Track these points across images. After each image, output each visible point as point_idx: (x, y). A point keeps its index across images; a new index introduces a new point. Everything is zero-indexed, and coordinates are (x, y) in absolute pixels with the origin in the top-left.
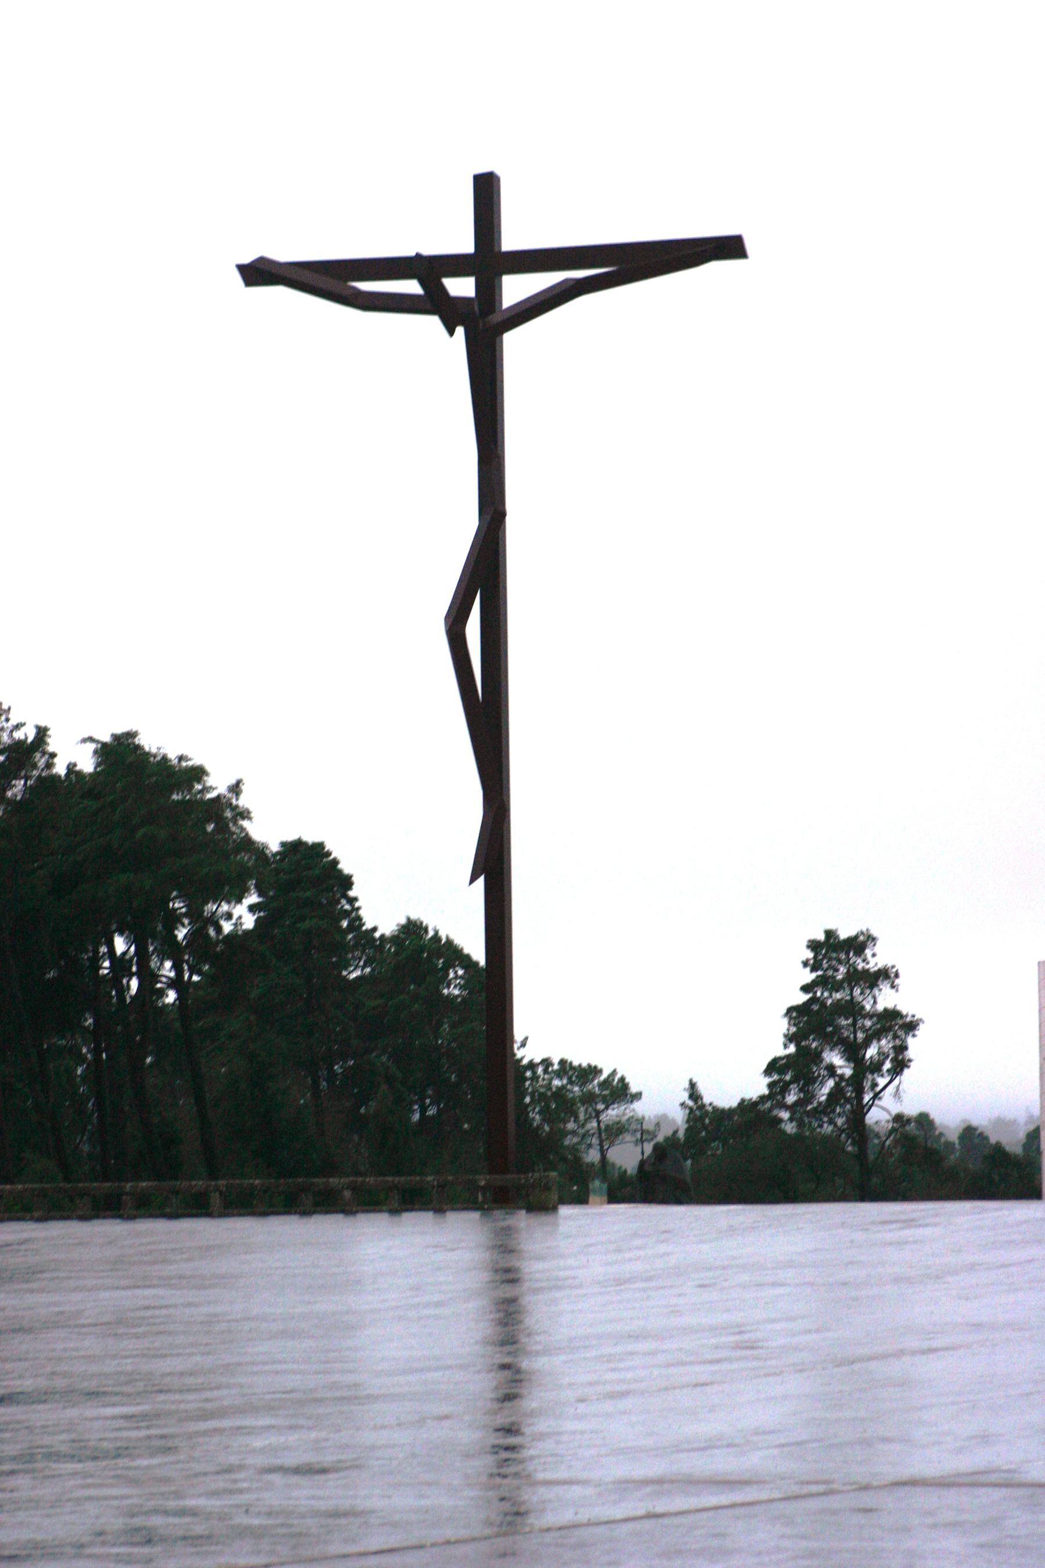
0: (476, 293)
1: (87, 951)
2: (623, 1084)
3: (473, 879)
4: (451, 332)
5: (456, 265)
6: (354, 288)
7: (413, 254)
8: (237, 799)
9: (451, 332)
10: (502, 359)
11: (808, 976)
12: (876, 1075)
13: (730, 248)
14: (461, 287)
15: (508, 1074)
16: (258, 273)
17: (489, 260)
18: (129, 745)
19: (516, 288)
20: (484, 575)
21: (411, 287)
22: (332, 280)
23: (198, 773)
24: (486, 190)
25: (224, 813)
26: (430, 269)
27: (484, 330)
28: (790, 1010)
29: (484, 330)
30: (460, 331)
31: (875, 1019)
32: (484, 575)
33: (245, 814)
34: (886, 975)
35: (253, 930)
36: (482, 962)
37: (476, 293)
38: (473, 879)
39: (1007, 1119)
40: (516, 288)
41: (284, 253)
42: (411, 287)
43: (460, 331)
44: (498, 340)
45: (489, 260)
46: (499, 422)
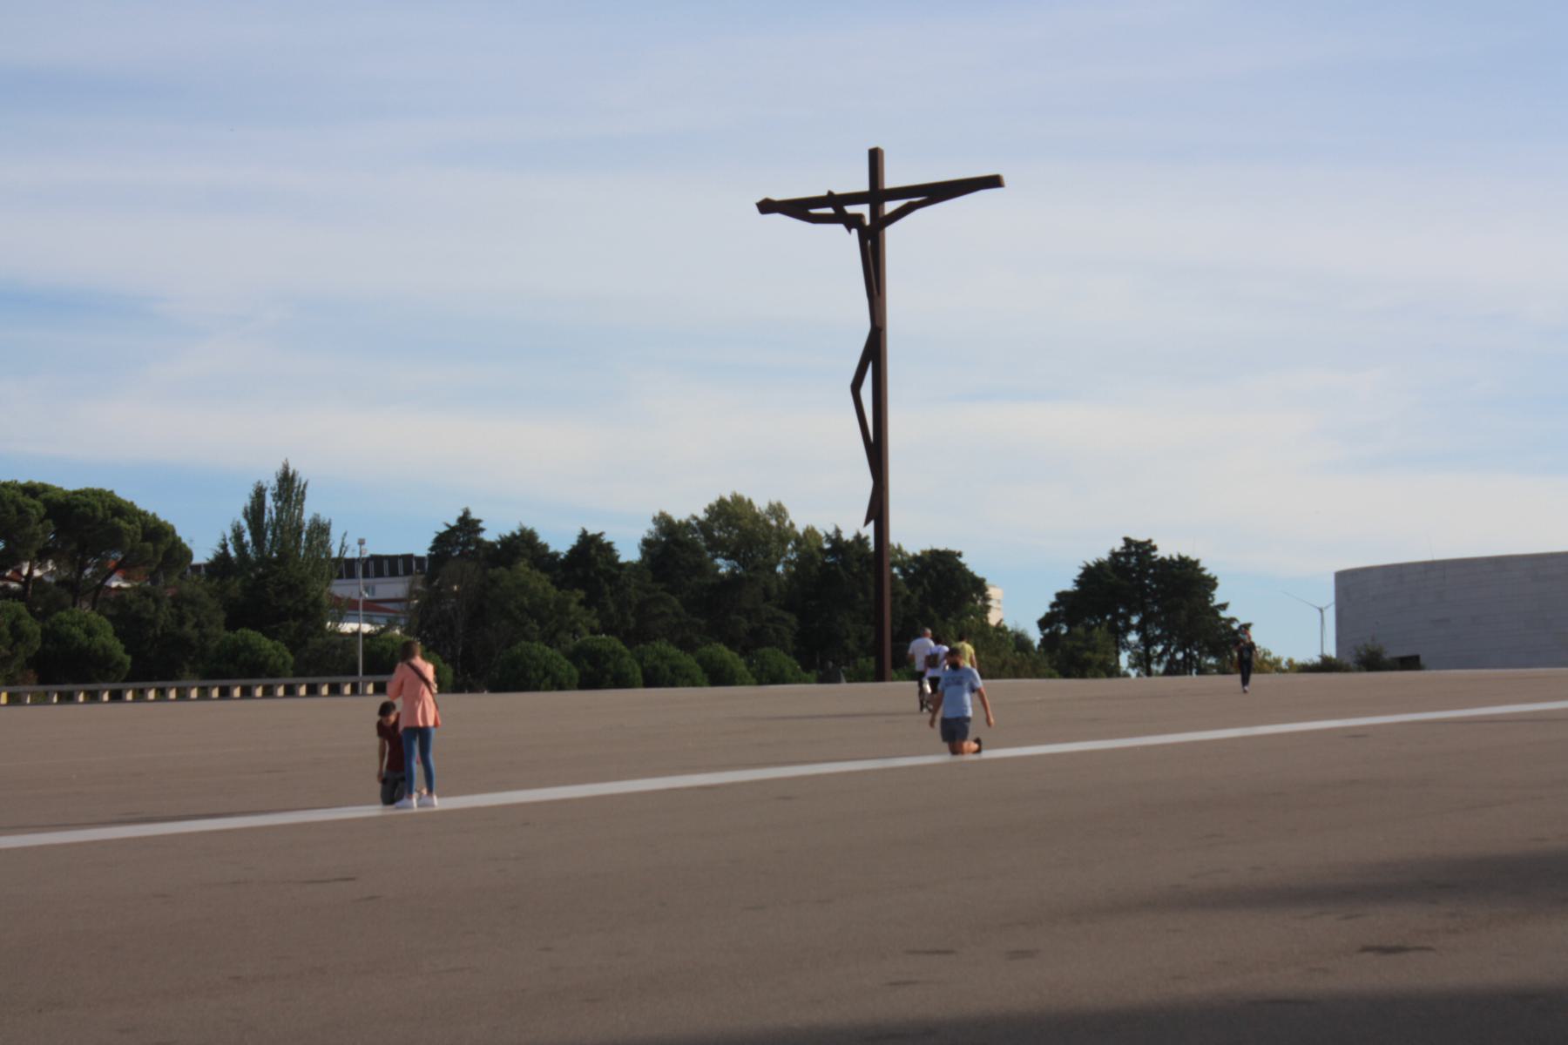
3: (867, 522)
7: (129, 500)
11: (702, 516)
13: (994, 182)
14: (864, 210)
16: (766, 207)
17: (876, 195)
19: (890, 207)
21: (830, 211)
22: (799, 209)
23: (1211, 583)
24: (875, 157)
26: (831, 199)
28: (1126, 540)
30: (855, 231)
35: (642, 561)
37: (869, 213)
38: (867, 522)
39: (249, 504)
40: (890, 207)
41: (778, 196)
42: (830, 211)
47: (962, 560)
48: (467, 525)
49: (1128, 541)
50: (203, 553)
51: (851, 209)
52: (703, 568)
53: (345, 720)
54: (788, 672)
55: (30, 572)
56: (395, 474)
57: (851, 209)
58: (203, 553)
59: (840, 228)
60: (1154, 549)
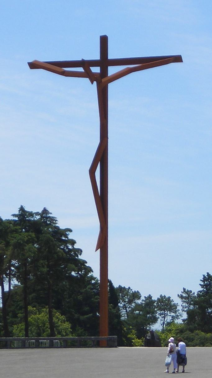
0: (100, 71)
1: (4, 248)
3: (96, 250)
4: (92, 83)
6: (98, 163)
7: (81, 59)
8: (166, 304)
9: (92, 83)
13: (178, 59)
14: (96, 70)
15: (104, 79)
16: (34, 65)
17: (105, 62)
20: (101, 157)
21: (81, 70)
22: (59, 67)
24: (104, 41)
25: (48, 211)
28: (150, 295)
30: (95, 83)
32: (101, 157)
33: (80, 251)
34: (208, 273)
37: (100, 71)
38: (96, 250)
40: (112, 70)
41: (43, 58)
42: (81, 70)
43: (95, 83)
45: (105, 62)
47: (71, 236)
49: (45, 211)
52: (20, 264)
53: (162, 355)
55: (13, 266)
56: (97, 141)
59: (86, 81)
60: (86, 263)
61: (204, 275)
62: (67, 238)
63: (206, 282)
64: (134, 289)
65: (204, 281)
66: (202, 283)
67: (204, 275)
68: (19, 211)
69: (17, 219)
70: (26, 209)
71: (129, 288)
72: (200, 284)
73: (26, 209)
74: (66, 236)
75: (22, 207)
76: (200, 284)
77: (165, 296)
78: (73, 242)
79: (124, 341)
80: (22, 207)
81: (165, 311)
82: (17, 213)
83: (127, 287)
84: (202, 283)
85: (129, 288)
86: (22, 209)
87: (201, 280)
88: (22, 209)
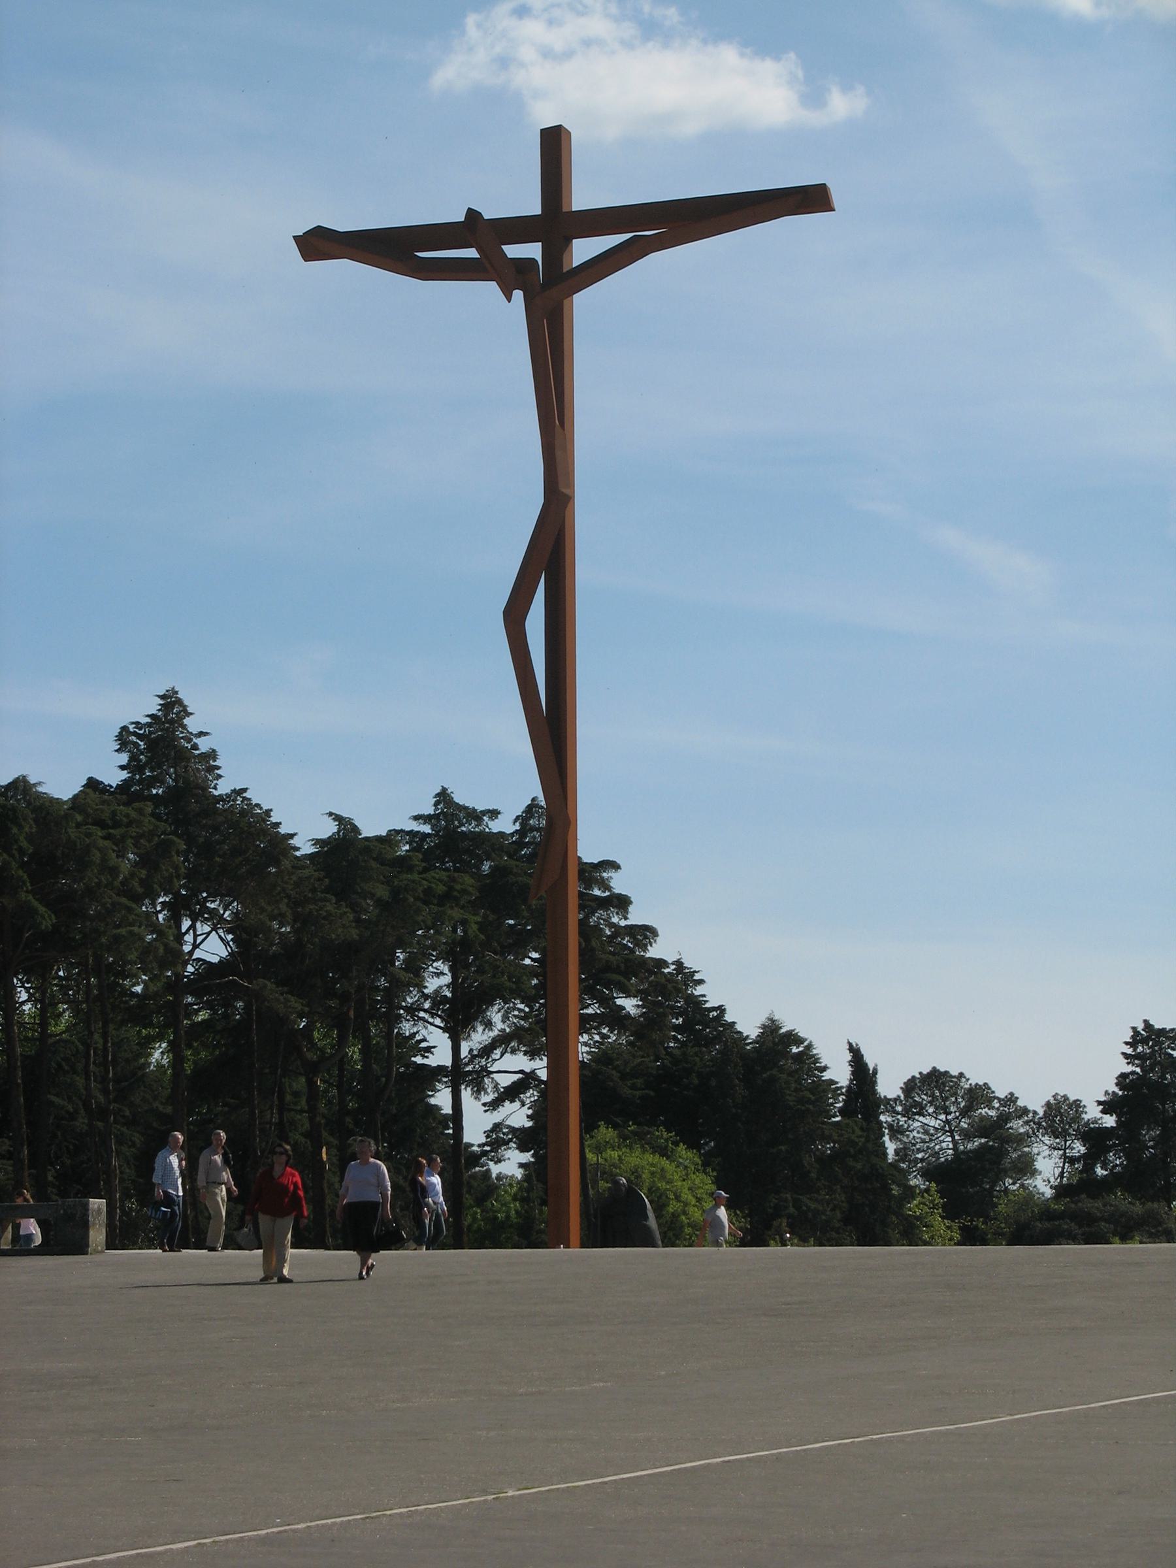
2: (438, 795)
5: (518, 229)
10: (565, 655)
12: (1018, 1126)
13: (811, 199)
14: (532, 251)
16: (318, 244)
17: (556, 222)
18: (520, 1189)
19: (584, 250)
20: (549, 557)
21: (471, 253)
22: (397, 249)
24: (554, 143)
26: (472, 227)
27: (548, 299)
28: (1012, 1094)
29: (548, 299)
30: (518, 295)
31: (248, 1218)
32: (549, 557)
33: (645, 934)
36: (565, 270)
37: (544, 253)
40: (584, 250)
42: (471, 253)
44: (566, 302)
45: (556, 222)
46: (568, 598)
47: (619, 883)
48: (631, 902)
49: (934, 1070)
50: (304, 847)
51: (513, 251)
54: (663, 1221)
57: (513, 251)
58: (304, 847)
61: (1134, 1029)
62: (608, 888)
63: (1140, 1049)
64: (975, 1077)
65: (1133, 1044)
66: (1129, 1051)
67: (1134, 1029)
68: (436, 804)
69: (426, 829)
70: (460, 798)
71: (961, 1075)
72: (1123, 1054)
73: (456, 800)
74: (604, 885)
75: (444, 790)
76: (1123, 1054)
77: (1065, 1098)
78: (622, 903)
79: (226, 1161)
80: (444, 790)
81: (1066, 1141)
82: (430, 810)
83: (954, 1073)
84: (1129, 1051)
85: (961, 1075)
86: (443, 797)
87: (1127, 1043)
88: (443, 797)
